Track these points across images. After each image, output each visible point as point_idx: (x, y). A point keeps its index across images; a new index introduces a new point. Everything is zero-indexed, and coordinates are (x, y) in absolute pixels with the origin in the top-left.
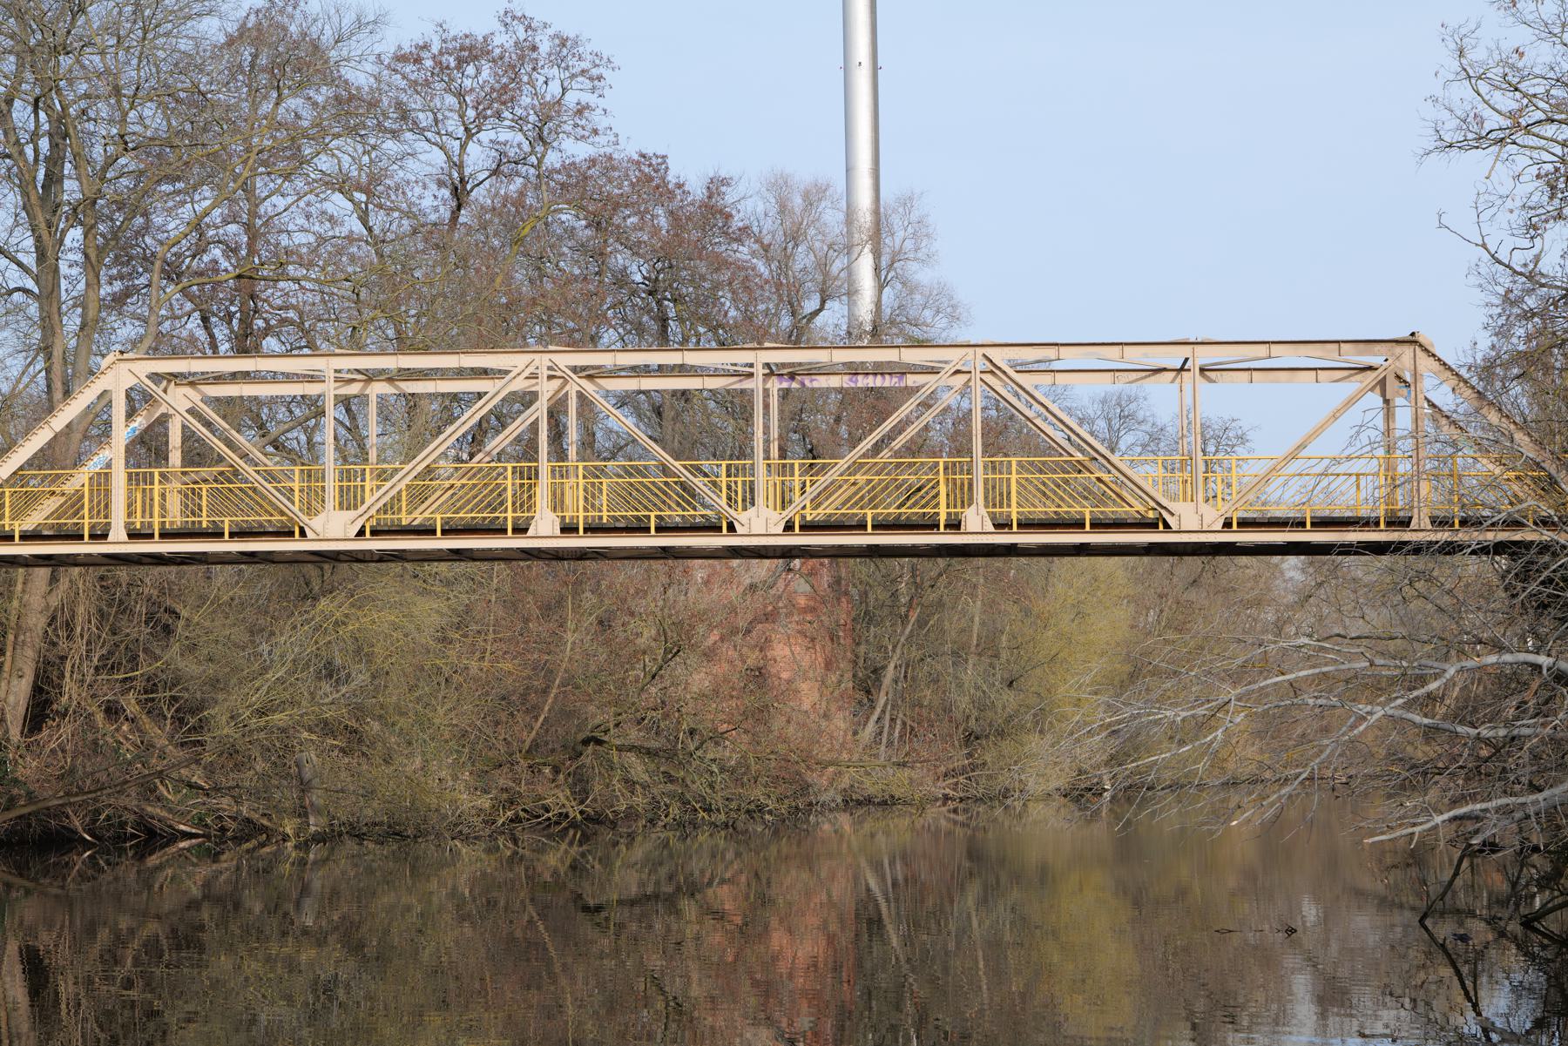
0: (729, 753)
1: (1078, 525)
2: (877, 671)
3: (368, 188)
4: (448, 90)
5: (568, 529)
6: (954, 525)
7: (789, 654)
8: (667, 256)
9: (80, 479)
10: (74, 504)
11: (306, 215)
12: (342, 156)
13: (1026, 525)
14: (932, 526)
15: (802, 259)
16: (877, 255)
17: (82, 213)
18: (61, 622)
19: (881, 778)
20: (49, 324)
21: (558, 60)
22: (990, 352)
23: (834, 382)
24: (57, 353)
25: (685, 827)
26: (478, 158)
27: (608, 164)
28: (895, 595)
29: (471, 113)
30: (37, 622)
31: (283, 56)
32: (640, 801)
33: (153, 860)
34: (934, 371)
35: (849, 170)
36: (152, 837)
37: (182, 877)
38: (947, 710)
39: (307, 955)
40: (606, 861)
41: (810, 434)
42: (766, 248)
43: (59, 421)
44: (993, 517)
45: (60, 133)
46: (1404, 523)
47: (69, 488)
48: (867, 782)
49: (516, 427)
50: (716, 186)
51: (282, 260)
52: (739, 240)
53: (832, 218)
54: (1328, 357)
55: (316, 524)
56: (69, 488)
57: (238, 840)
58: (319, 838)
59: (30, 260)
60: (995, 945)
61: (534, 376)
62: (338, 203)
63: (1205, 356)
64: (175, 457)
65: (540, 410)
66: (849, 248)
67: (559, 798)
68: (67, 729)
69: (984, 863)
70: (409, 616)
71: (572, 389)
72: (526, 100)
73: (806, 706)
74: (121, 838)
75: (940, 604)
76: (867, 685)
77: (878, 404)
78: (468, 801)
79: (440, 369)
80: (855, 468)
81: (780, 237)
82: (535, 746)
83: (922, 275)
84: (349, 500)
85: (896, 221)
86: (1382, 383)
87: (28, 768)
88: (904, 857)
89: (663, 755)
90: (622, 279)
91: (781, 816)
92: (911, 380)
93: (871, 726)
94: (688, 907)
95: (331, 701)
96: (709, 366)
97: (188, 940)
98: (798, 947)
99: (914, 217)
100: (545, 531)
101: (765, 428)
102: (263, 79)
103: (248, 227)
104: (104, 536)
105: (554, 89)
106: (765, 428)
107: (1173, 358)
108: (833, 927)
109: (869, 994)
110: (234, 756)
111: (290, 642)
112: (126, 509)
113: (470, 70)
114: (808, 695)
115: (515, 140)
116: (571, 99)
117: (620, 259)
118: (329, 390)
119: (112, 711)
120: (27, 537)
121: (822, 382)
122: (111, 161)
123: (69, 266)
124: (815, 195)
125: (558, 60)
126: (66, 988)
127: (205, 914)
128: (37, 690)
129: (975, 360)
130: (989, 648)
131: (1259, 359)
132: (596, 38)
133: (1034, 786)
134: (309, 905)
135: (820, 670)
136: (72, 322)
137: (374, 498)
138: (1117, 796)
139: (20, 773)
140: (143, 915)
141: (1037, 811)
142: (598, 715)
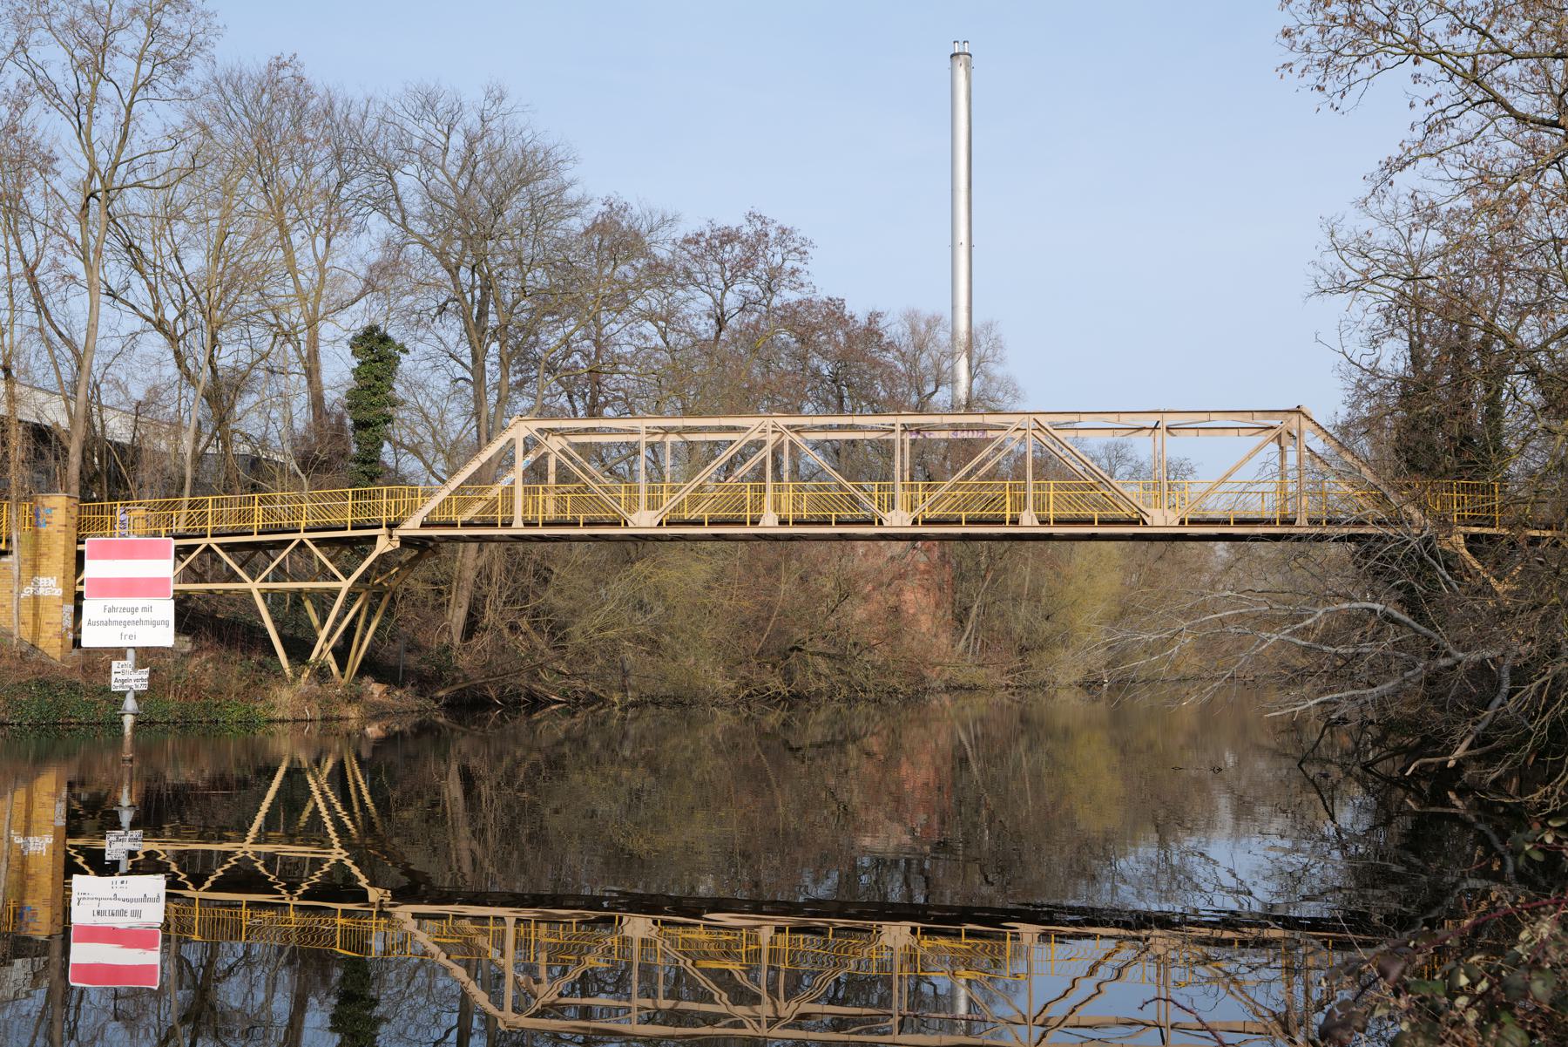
2: (967, 609)
3: (666, 319)
4: (715, 260)
5: (783, 522)
6: (1015, 522)
7: (914, 598)
8: (844, 359)
9: (496, 491)
10: (493, 505)
11: (630, 335)
12: (651, 299)
13: (1059, 522)
14: (1002, 522)
15: (925, 361)
16: (970, 359)
17: (500, 333)
18: (484, 575)
19: (970, 673)
20: (479, 399)
21: (781, 242)
22: (1038, 417)
24: (484, 416)
25: (851, 701)
26: (732, 301)
27: (809, 304)
28: (978, 564)
29: (728, 274)
30: (470, 575)
31: (617, 237)
32: (823, 685)
33: (536, 716)
34: (1003, 429)
35: (954, 308)
36: (536, 703)
37: (552, 726)
40: (803, 721)
42: (903, 355)
43: (484, 457)
44: (1038, 517)
45: (487, 287)
46: (1292, 522)
48: (960, 676)
49: (753, 462)
50: (874, 317)
51: (616, 360)
52: (887, 350)
53: (943, 337)
54: (1245, 421)
56: (490, 496)
57: (586, 705)
58: (634, 705)
59: (468, 361)
61: (764, 431)
62: (649, 328)
63: (1170, 420)
64: (552, 478)
65: (767, 451)
66: (953, 355)
67: (775, 683)
68: (487, 638)
69: (1029, 725)
71: (786, 439)
72: (761, 266)
73: (924, 630)
74: (518, 703)
76: (961, 617)
78: (722, 683)
80: (956, 487)
81: (912, 348)
82: (761, 652)
83: (997, 371)
84: (653, 504)
85: (982, 339)
86: (1279, 437)
87: (464, 661)
88: (982, 720)
89: (839, 658)
90: (816, 373)
91: (908, 695)
92: (990, 434)
93: (963, 643)
94: (852, 749)
95: (641, 624)
96: (868, 425)
97: (556, 765)
98: (917, 774)
99: (993, 336)
100: (769, 523)
101: (901, 462)
102: (606, 254)
103: (596, 342)
104: (510, 525)
106: (901, 462)
107: (1150, 421)
108: (939, 762)
109: (960, 803)
110: (585, 655)
111: (618, 588)
112: (522, 508)
113: (728, 248)
114: (925, 623)
115: (754, 290)
116: (788, 265)
117: (816, 361)
118: (643, 439)
119: (513, 628)
120: (464, 525)
121: (936, 435)
122: (516, 303)
124: (932, 323)
126: (485, 790)
128: (470, 615)
129: (1028, 422)
130: (1035, 596)
133: (1062, 679)
134: (628, 745)
135: (932, 608)
136: (492, 398)
137: (668, 503)
138: (1113, 687)
139: (460, 664)
140: (530, 749)
141: (1063, 694)
142: (799, 634)
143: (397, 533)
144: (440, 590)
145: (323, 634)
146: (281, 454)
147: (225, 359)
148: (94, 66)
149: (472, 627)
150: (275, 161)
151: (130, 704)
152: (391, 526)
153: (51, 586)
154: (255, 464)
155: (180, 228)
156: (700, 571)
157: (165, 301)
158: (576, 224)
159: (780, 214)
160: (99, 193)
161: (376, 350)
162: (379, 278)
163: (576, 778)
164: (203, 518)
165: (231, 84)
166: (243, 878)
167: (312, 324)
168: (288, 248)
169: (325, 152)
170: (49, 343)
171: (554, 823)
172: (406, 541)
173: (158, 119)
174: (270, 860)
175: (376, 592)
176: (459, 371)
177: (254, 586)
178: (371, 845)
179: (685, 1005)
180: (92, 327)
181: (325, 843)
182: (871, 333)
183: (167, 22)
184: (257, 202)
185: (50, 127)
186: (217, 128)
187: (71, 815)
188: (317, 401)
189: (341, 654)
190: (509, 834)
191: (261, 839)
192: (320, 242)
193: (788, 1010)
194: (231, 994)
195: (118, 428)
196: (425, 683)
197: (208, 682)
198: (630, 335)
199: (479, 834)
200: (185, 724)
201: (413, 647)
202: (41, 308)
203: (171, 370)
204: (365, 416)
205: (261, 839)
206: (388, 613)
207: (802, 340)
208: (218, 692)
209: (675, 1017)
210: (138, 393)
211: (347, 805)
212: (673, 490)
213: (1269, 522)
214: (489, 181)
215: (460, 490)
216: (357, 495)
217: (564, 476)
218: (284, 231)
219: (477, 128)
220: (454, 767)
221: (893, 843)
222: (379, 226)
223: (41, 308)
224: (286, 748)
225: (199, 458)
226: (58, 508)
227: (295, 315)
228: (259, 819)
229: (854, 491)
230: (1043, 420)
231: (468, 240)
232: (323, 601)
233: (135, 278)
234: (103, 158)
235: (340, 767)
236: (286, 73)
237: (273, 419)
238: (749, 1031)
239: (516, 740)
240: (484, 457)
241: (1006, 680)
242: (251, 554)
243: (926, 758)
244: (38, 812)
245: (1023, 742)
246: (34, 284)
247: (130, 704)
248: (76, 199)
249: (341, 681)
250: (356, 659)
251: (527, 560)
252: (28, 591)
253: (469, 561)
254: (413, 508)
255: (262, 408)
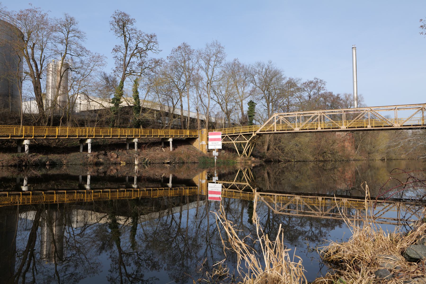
0: (340, 154)
1: (382, 127)
2: (357, 146)
3: (300, 97)
5: (322, 129)
6: (366, 127)
9: (272, 126)
11: (294, 100)
12: (298, 94)
13: (375, 127)
14: (364, 127)
15: (348, 102)
16: (357, 101)
17: (272, 101)
18: (270, 140)
19: (359, 157)
20: (269, 112)
21: (320, 82)
22: (371, 108)
23: (352, 112)
26: (312, 93)
27: (326, 93)
30: (268, 140)
31: (291, 84)
32: (330, 159)
35: (354, 93)
36: (279, 161)
37: (282, 165)
38: (366, 150)
39: (295, 173)
41: (349, 117)
43: (269, 120)
45: (269, 94)
47: (271, 126)
49: (316, 119)
50: (338, 95)
54: (415, 106)
55: (295, 129)
56: (271, 126)
58: (296, 162)
60: (372, 176)
63: (398, 107)
64: (281, 123)
65: (319, 117)
67: (321, 158)
68: (271, 151)
70: (304, 139)
71: (322, 115)
75: (365, 139)
77: (357, 115)
78: (312, 158)
79: (307, 113)
82: (318, 153)
84: (298, 127)
85: (359, 97)
87: (267, 154)
89: (333, 154)
90: (328, 105)
94: (336, 170)
95: (297, 148)
96: (336, 112)
97: (283, 172)
98: (349, 175)
100: (319, 129)
101: (344, 116)
105: (320, 85)
106: (344, 116)
107: (394, 107)
109: (357, 180)
110: (287, 154)
111: (293, 142)
112: (276, 128)
114: (349, 149)
115: (316, 91)
117: (327, 103)
118: (296, 116)
119: (275, 149)
121: (350, 112)
123: (270, 107)
124: (350, 95)
125: (320, 82)
126: (271, 176)
127: (285, 169)
128: (268, 147)
130: (371, 144)
131: (406, 107)
132: (324, 79)
133: (377, 159)
136: (271, 112)
137: (301, 126)
138: (388, 160)
140: (279, 169)
141: (377, 161)
142: (325, 150)
143: (256, 133)
144: (263, 143)
145: (244, 150)
146: (238, 122)
147: (229, 107)
148: (208, 62)
149: (268, 149)
150: (235, 76)
151: (216, 158)
152: (255, 132)
153: (204, 143)
154: (233, 124)
155: (221, 87)
156: (307, 139)
157: (219, 99)
158: (284, 82)
159: (320, 78)
160: (209, 83)
161: (252, 104)
162: (252, 92)
163: (286, 173)
164: (226, 132)
165: (228, 65)
166: (233, 187)
167: (242, 101)
168: (238, 90)
169: (243, 73)
170: (203, 107)
171: (283, 182)
172: (257, 134)
173: (217, 70)
174: (238, 185)
175: (253, 143)
176: (265, 108)
177: (234, 142)
178: (253, 183)
179: (306, 211)
180: (209, 103)
181: (246, 182)
182: (338, 97)
183: (218, 55)
184: (233, 83)
185: (202, 73)
186: (226, 72)
187: (208, 177)
188: (243, 114)
189: (247, 153)
190: (275, 183)
191: (236, 181)
192: (243, 88)
193: (325, 213)
194: (232, 206)
195: (213, 120)
196: (261, 158)
197: (227, 157)
198: (294, 100)
199: (270, 183)
200: (224, 163)
201: (259, 152)
202: (202, 101)
203: (221, 110)
204: (250, 115)
205: (236, 181)
206: (255, 146)
207: (325, 99)
208: (229, 158)
209: (304, 213)
210: (216, 113)
211: (249, 177)
212: (302, 124)
213: (420, 125)
214: (269, 76)
215: (266, 126)
216: (249, 127)
217: (283, 122)
218: (237, 87)
219: (267, 68)
220: (266, 171)
221: (344, 187)
222: (252, 85)
223: (202, 101)
224: (239, 167)
225: (225, 123)
226: (205, 130)
227: (239, 100)
228: (235, 179)
229: (335, 123)
230: (372, 109)
231: (266, 86)
232: (244, 144)
233: (215, 96)
234: (210, 78)
235: (248, 170)
236: (236, 61)
237: (236, 117)
238: (317, 216)
239: (276, 167)
240: (269, 120)
241: (366, 159)
242: (233, 137)
243: (350, 172)
244: (203, 177)
245: (369, 170)
246: (200, 98)
247: (216, 158)
248: (206, 84)
249: (248, 157)
250: (250, 154)
251: (277, 137)
252: (201, 143)
253: (268, 138)
254: (258, 129)
255: (234, 114)
